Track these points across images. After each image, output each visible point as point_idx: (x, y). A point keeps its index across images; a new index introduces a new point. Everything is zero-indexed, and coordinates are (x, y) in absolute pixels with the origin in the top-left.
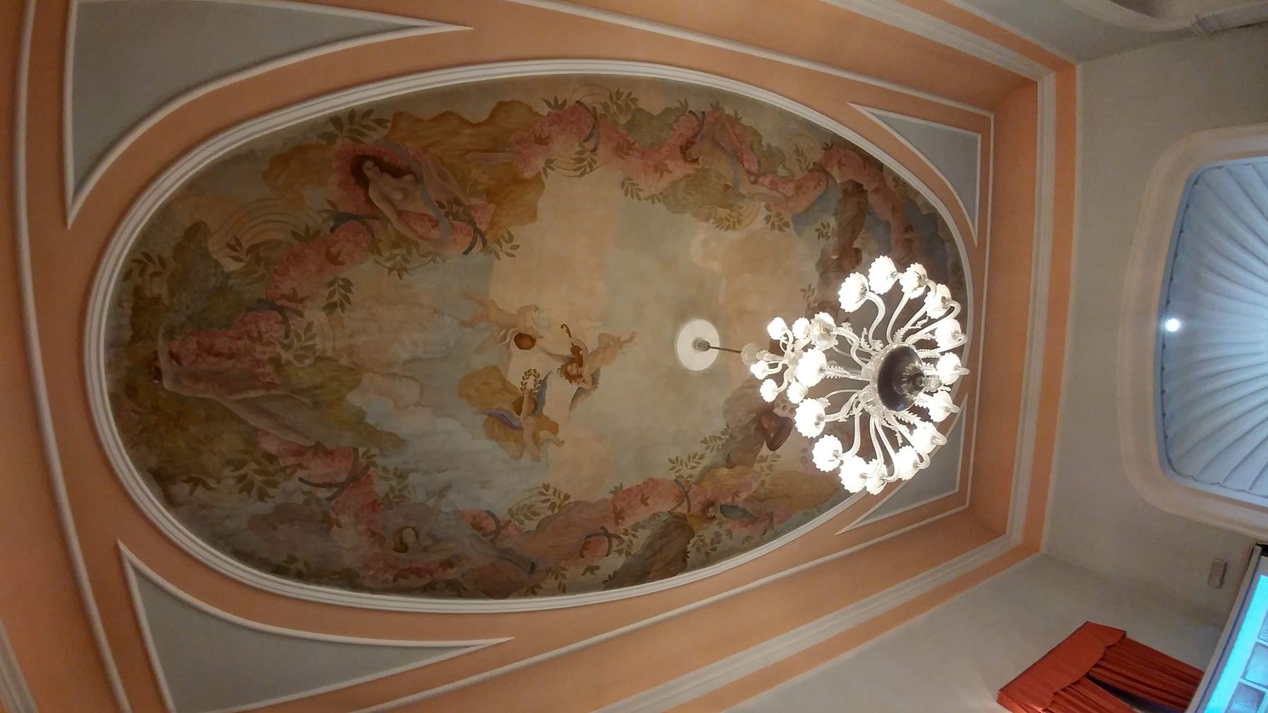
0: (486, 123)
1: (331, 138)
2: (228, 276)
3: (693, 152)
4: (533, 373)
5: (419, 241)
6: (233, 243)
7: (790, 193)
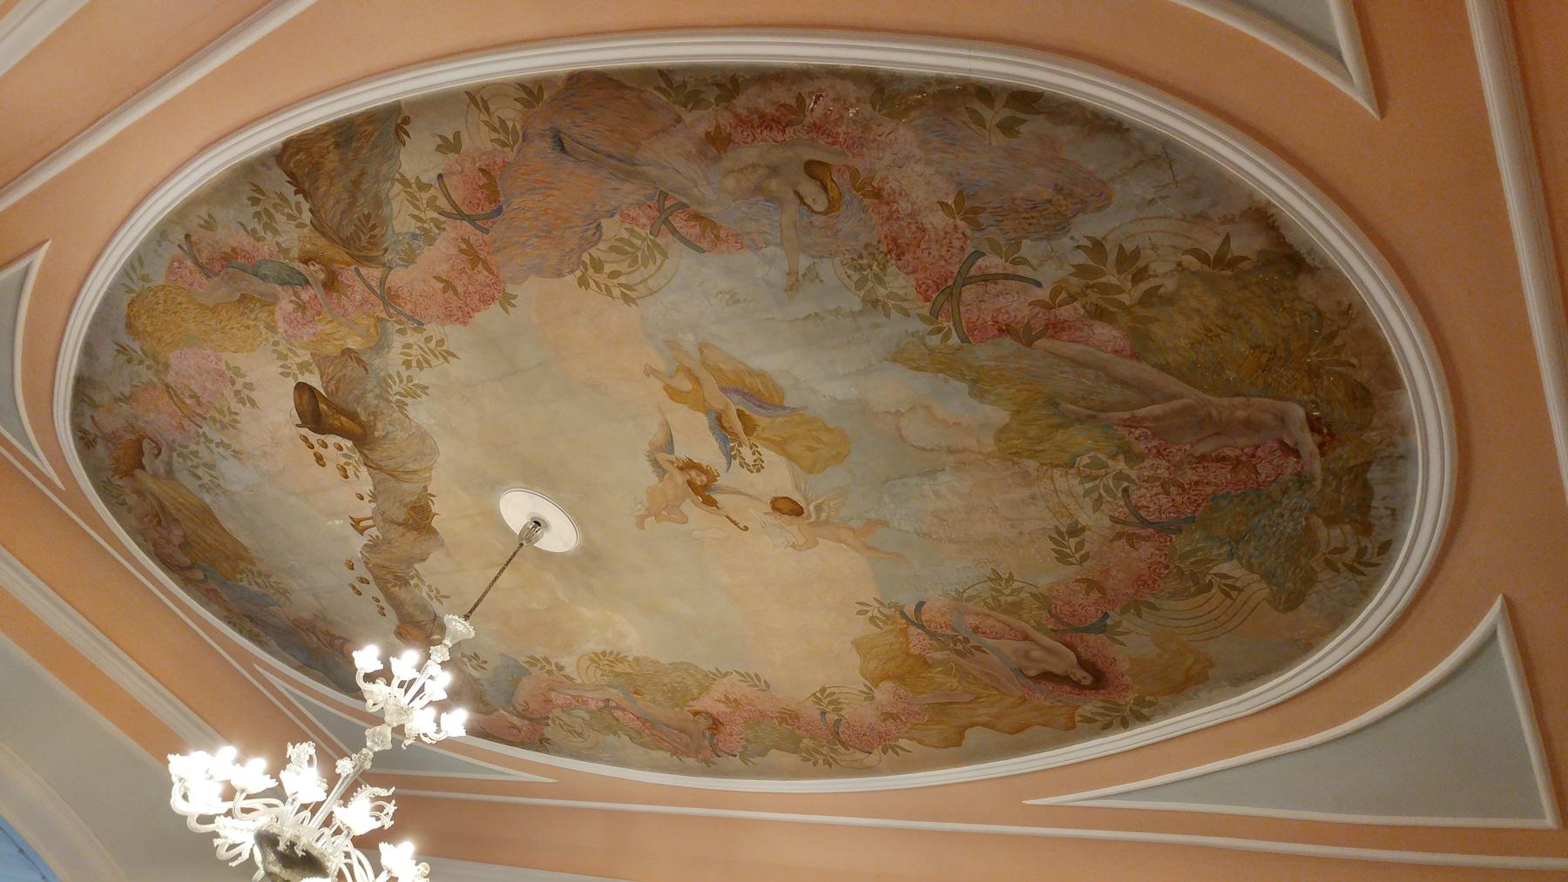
0: (966, 727)
1: (1140, 701)
2: (1231, 556)
3: (704, 723)
4: (752, 468)
5: (987, 611)
6: (1234, 594)
7: (553, 695)
